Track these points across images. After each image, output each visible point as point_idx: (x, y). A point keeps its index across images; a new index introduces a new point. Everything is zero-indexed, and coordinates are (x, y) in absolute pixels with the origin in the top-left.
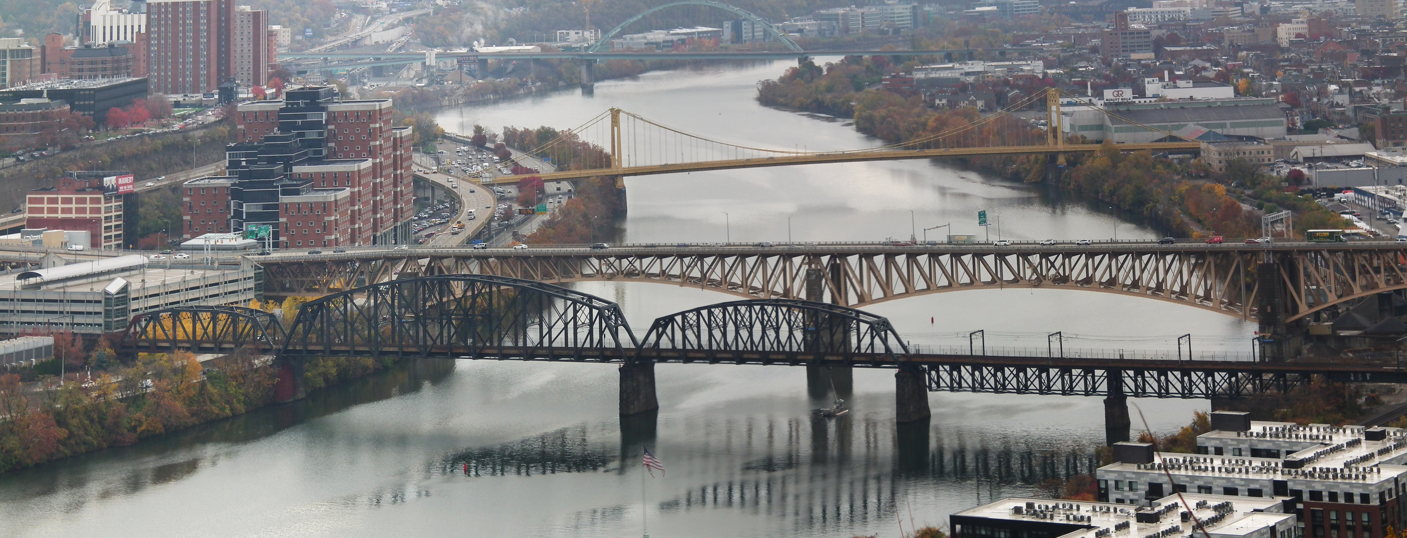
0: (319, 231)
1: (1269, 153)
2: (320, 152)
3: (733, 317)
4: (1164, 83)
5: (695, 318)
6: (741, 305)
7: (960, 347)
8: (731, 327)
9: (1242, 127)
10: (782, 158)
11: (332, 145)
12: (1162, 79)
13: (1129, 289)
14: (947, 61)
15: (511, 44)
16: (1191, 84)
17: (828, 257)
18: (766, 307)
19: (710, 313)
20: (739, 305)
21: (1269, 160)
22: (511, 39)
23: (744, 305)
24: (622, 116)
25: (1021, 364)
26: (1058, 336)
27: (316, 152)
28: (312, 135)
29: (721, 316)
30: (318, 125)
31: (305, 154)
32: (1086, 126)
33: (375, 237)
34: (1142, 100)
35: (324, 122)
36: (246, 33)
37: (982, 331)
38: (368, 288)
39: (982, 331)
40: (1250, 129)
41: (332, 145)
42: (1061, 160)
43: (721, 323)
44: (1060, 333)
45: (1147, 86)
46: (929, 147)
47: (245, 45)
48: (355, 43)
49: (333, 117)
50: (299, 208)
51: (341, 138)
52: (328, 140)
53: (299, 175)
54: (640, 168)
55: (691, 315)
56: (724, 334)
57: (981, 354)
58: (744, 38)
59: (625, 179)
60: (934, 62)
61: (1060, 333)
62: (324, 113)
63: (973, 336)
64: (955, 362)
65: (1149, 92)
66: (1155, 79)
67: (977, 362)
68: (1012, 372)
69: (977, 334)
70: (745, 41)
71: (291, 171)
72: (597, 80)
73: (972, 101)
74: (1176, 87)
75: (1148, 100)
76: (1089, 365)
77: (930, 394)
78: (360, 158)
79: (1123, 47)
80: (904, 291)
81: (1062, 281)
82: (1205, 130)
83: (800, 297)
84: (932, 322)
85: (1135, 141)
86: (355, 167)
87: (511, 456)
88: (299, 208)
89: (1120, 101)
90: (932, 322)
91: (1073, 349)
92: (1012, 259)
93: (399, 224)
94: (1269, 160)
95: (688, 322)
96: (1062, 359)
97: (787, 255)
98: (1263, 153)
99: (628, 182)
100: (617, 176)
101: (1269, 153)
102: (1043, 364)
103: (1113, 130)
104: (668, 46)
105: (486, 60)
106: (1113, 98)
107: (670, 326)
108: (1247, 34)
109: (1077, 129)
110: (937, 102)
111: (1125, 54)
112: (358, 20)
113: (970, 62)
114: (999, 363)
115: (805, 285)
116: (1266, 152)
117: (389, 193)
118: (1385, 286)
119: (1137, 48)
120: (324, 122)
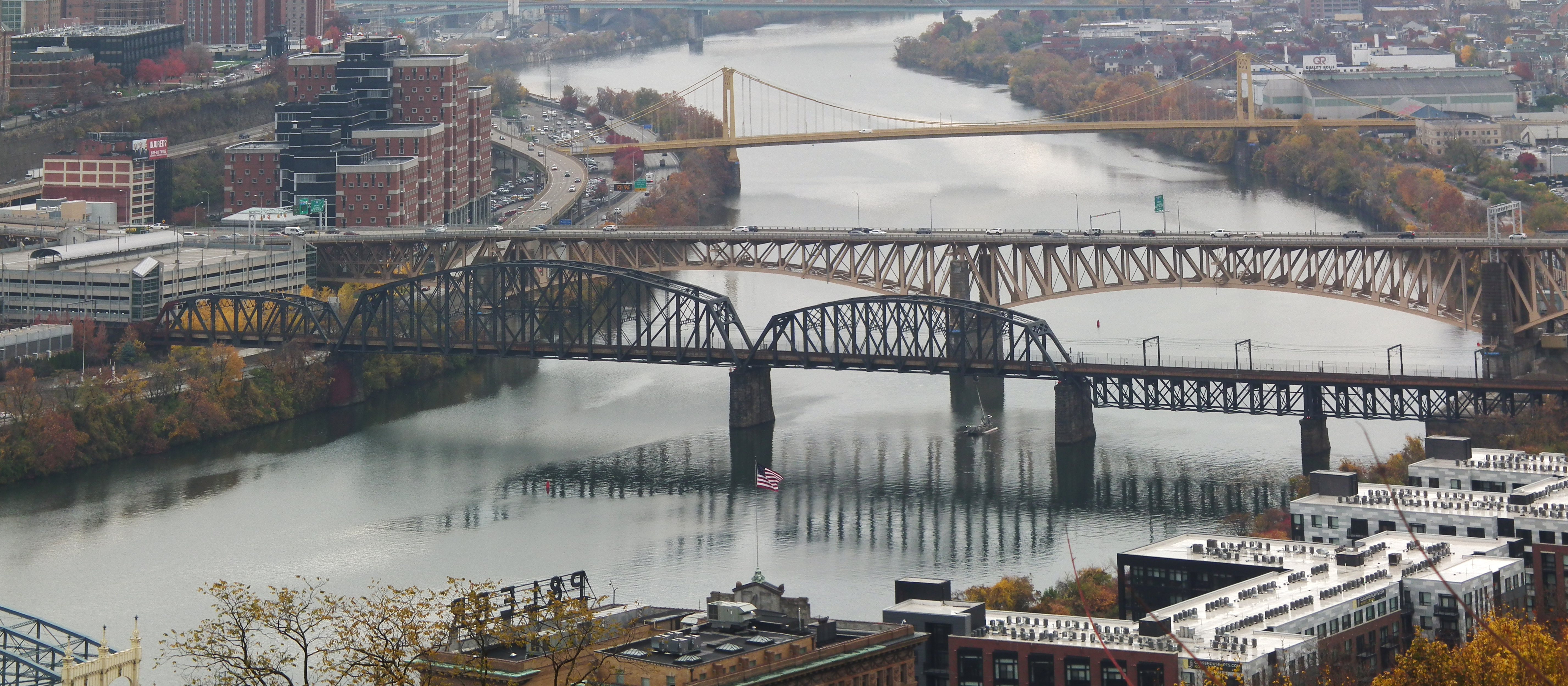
1: (1496, 133)
3: (864, 315)
5: (819, 316)
7: (1132, 356)
8: (861, 328)
14: (1119, 17)
16: (1405, 51)
19: (837, 311)
24: (736, 78)
25: (1203, 377)
26: (1247, 345)
27: (379, 115)
28: (374, 94)
29: (849, 313)
30: (381, 83)
33: (447, 215)
34: (1348, 69)
35: (389, 80)
41: (398, 106)
43: (849, 323)
44: (1249, 341)
49: (399, 74)
51: (408, 98)
52: (393, 100)
55: (814, 312)
56: (853, 336)
57: (1156, 364)
60: (1104, 18)
61: (1249, 341)
62: (389, 69)
63: (1147, 344)
64: (1125, 374)
65: (1356, 60)
71: (350, 136)
73: (1149, 66)
76: (1282, 380)
80: (1066, 289)
81: (1252, 279)
85: (1339, 117)
89: (1322, 69)
95: (811, 321)
96: (1251, 372)
98: (1489, 133)
101: (1496, 133)
102: (1228, 378)
103: (1314, 103)
105: (578, 10)
106: (1314, 65)
110: (1107, 66)
113: (1146, 20)
114: (1177, 376)
116: (1492, 132)
120: (389, 80)
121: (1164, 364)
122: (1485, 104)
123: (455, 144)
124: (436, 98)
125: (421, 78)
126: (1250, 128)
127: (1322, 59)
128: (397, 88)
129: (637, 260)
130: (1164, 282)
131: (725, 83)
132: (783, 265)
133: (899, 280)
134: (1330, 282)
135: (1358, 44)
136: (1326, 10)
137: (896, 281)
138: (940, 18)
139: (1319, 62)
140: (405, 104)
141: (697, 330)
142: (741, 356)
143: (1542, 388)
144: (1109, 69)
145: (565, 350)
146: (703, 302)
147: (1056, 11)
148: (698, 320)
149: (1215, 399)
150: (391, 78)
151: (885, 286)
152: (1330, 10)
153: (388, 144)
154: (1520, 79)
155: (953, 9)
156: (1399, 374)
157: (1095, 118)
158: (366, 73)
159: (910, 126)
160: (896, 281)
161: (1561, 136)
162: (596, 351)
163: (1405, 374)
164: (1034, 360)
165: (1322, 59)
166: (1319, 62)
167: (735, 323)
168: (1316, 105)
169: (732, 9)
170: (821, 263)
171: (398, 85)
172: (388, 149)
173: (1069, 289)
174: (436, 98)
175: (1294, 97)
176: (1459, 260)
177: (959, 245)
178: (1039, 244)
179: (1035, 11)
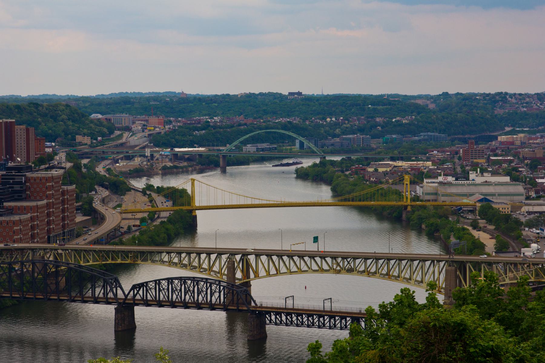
0: (11, 234)
1: (508, 209)
2: (21, 196)
4: (477, 174)
5: (166, 284)
6: (176, 279)
7: (279, 303)
9: (520, 196)
10: (273, 204)
11: (29, 193)
12: (477, 172)
13: (384, 276)
14: (389, 160)
15: (195, 147)
16: (490, 175)
17: (240, 255)
18: (187, 281)
20: (174, 279)
21: (508, 212)
22: (195, 145)
23: (177, 280)
24: (196, 182)
25: (310, 313)
26: (330, 300)
27: (19, 196)
28: (17, 187)
30: (20, 183)
31: (13, 197)
32: (430, 193)
33: (49, 238)
34: (468, 182)
35: (23, 182)
36: (23, 138)
37: (293, 296)
38: (20, 262)
39: (293, 296)
40: (507, 197)
41: (29, 193)
42: (409, 208)
44: (331, 299)
45: (470, 175)
46: (349, 201)
47: (23, 144)
48: (122, 145)
49: (28, 180)
50: (14, 222)
51: (32, 189)
52: (26, 190)
53: (7, 207)
54: (226, 206)
55: (164, 282)
57: (292, 307)
58: (305, 147)
59: (197, 211)
60: (383, 160)
61: (331, 299)
62: (23, 178)
63: (287, 299)
64: (278, 312)
65: (471, 178)
66: (474, 172)
67: (289, 312)
68: (306, 316)
69: (289, 298)
70: (305, 149)
71: (3, 205)
72: (229, 165)
73: (387, 179)
74: (483, 176)
75: (471, 182)
76: (343, 316)
77: (267, 326)
78: (41, 200)
79: (471, 157)
80: (276, 273)
81: (350, 271)
82: (483, 197)
83: (225, 273)
84: (306, 288)
85: (451, 202)
86: (40, 203)
87: (230, 329)
88: (14, 222)
89: (446, 182)
90: (306, 288)
91: (337, 306)
92: (329, 260)
93: (66, 230)
94: (508, 212)
96: (331, 311)
97: (220, 254)
98: (505, 209)
99: (198, 213)
100: (193, 210)
101: (508, 209)
102: (321, 314)
103: (441, 195)
104: (267, 150)
105: (178, 154)
106: (442, 180)
107: (142, 289)
108: (531, 152)
109: (424, 194)
110: (372, 179)
111: (472, 160)
112: (126, 135)
113: (398, 161)
114: (299, 313)
115: (227, 269)
116: (506, 208)
117: (59, 216)
118: (509, 280)
119: (481, 157)
120: (23, 182)
121: (333, 310)
122: (512, 197)
123: (53, 208)
124: (44, 189)
125: (38, 181)
126: (408, 205)
127: (446, 178)
128: (28, 185)
129: (91, 257)
130: (315, 271)
131: (192, 185)
132: (367, 272)
133: (219, 271)
134: (384, 272)
135: (472, 172)
136: (471, 159)
137: (218, 271)
138: (318, 161)
139: (445, 179)
140: (31, 192)
141: (220, 296)
142: (120, 301)
143: (335, 314)
144: (372, 180)
145: (72, 298)
146: (209, 283)
147: (173, 154)
148: (220, 292)
149: (315, 323)
150: (24, 181)
151: (201, 270)
152: (473, 159)
153: (31, 208)
154: (531, 187)
155: (325, 156)
156: (323, 310)
157: (345, 200)
158: (14, 179)
159: (268, 202)
160: (218, 271)
161: (534, 211)
162: (85, 299)
163: (287, 307)
164: (326, 310)
165: (446, 178)
166: (445, 179)
167: (119, 287)
168: (442, 196)
169: (247, 155)
170: (176, 260)
171: (28, 184)
172: (19, 210)
173: (277, 273)
174: (44, 189)
175: (431, 193)
176: (469, 266)
177: (232, 253)
178: (430, 260)
179: (235, 156)
